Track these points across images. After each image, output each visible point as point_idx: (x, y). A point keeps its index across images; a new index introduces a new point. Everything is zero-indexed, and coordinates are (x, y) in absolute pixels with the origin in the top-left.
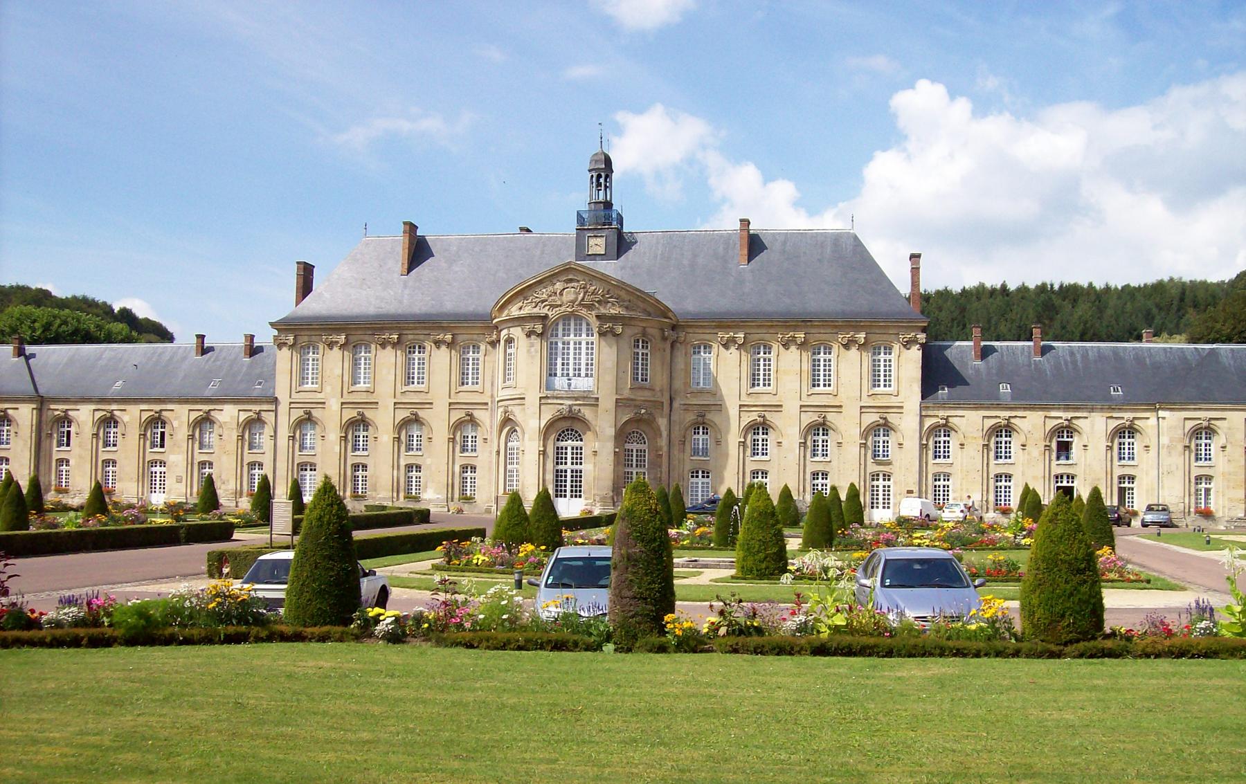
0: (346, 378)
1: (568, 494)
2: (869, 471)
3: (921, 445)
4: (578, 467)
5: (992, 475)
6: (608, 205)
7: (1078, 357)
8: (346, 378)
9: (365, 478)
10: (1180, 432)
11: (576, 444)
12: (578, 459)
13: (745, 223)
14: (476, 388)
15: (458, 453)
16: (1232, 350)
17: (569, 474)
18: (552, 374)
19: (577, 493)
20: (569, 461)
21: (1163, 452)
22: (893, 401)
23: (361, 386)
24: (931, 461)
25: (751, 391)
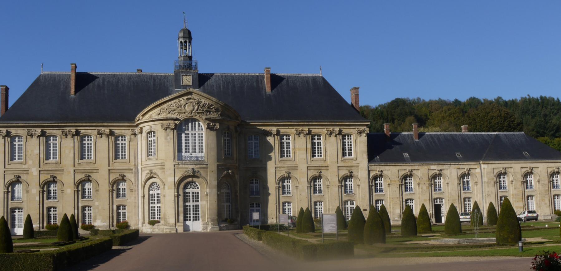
0: (42, 156)
1: (191, 218)
2: (343, 200)
3: (369, 186)
4: (197, 203)
5: (404, 200)
6: (190, 58)
7: (436, 139)
8: (42, 156)
9: (124, 214)
10: (492, 175)
11: (195, 190)
12: (196, 199)
13: (268, 69)
14: (90, 160)
15: (115, 199)
16: (505, 135)
17: (191, 207)
18: (180, 150)
19: (196, 218)
20: (191, 200)
21: (485, 185)
22: (354, 163)
23: (51, 160)
24: (374, 194)
25: (343, 159)
